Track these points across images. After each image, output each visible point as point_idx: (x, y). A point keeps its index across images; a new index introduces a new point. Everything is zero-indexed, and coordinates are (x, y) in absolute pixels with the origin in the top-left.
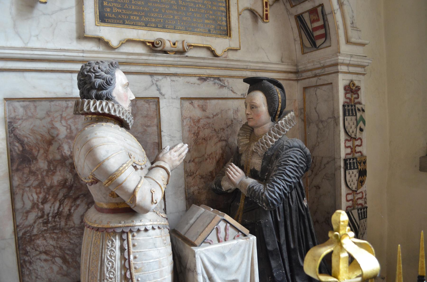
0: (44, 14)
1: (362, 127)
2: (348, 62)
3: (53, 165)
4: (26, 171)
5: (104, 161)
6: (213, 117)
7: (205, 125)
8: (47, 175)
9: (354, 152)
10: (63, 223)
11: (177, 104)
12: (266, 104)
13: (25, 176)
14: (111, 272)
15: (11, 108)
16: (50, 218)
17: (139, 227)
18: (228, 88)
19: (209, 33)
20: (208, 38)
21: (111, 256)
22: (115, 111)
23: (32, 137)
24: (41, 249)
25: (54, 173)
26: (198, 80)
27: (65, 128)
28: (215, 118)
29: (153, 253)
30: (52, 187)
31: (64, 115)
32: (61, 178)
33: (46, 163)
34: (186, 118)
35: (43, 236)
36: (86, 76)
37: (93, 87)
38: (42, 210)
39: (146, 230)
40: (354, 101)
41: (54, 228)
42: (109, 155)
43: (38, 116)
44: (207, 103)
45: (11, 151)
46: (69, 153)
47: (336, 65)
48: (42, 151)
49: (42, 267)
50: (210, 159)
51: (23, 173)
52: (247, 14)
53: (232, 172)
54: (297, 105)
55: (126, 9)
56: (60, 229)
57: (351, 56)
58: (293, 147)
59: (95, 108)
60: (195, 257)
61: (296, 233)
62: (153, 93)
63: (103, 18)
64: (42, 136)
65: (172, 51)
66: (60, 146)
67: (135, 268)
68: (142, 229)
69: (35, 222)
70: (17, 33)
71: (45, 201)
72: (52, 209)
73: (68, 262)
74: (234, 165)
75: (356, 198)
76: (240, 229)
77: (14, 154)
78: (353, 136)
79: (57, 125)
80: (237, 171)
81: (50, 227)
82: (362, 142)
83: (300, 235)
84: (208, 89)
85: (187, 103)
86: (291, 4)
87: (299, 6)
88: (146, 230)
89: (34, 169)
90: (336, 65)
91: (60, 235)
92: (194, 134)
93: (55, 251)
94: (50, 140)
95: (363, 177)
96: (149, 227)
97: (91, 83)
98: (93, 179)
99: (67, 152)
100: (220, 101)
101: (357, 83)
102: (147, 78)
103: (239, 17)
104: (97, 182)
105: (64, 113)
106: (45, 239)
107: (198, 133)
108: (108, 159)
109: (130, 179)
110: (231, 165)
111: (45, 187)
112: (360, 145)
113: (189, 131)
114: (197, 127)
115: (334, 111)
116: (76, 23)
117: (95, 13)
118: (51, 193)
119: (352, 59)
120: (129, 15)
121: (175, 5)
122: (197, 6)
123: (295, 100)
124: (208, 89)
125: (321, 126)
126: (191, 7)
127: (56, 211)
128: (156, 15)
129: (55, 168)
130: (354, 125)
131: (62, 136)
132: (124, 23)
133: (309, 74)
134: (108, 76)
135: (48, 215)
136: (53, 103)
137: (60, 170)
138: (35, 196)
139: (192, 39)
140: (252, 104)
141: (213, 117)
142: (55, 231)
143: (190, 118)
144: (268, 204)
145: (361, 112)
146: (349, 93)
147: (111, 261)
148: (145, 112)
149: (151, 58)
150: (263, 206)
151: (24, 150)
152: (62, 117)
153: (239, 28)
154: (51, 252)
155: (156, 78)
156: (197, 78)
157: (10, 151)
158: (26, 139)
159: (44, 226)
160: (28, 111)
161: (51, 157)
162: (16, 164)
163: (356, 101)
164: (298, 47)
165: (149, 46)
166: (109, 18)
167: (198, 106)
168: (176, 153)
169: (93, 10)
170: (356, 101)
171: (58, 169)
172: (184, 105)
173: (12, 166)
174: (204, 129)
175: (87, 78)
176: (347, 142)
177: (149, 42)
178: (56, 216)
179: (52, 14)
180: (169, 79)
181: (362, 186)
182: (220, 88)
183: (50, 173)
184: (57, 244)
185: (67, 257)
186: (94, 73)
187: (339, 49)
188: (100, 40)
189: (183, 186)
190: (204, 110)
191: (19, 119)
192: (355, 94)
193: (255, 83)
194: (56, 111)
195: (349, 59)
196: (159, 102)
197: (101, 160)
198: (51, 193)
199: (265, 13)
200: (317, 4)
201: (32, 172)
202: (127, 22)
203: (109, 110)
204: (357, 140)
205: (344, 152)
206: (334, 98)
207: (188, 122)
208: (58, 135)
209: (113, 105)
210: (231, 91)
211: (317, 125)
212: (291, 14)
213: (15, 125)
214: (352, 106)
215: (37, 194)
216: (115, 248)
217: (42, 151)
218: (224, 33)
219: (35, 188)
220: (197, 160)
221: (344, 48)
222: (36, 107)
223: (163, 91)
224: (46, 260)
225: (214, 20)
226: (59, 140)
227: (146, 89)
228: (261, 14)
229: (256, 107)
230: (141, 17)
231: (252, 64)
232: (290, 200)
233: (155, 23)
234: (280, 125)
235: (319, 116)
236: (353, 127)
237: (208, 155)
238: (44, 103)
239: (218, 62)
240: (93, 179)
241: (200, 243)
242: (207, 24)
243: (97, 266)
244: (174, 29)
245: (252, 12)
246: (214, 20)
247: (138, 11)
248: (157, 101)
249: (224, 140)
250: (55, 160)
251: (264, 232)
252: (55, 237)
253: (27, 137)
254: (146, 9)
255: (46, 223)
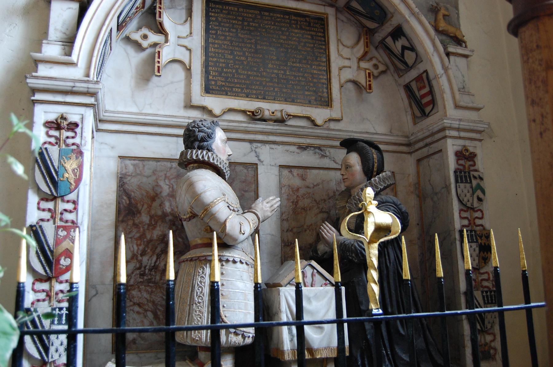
0: (157, 86)
1: (481, 196)
2: (457, 126)
3: (154, 220)
4: (131, 223)
5: (201, 194)
6: (314, 187)
7: (304, 194)
8: (148, 229)
9: (472, 224)
10: (158, 278)
11: (276, 170)
12: (360, 164)
13: (129, 227)
14: (200, 296)
15: (123, 165)
16: (147, 271)
17: (228, 258)
18: (330, 158)
19: (309, 103)
20: (307, 108)
21: (201, 282)
22: (213, 159)
23: (138, 193)
24: (136, 300)
25: (154, 228)
26: (298, 148)
27: (168, 186)
28: (315, 188)
29: (240, 284)
30: (151, 240)
31: (168, 175)
32: (160, 233)
33: (149, 217)
34: (285, 185)
35: (139, 287)
36: (191, 130)
37: (196, 139)
38: (140, 262)
39: (234, 262)
40: (469, 168)
41: (149, 281)
42: (206, 189)
43: (146, 174)
44: (307, 172)
45: (119, 203)
46: (170, 210)
47: (443, 129)
48: (145, 206)
49: (134, 319)
50: (310, 231)
51: (127, 225)
52: (350, 86)
53: (325, 231)
54: (411, 180)
55: (229, 82)
56: (154, 283)
57: (460, 120)
58: (386, 203)
59: (197, 156)
60: (279, 294)
61: (394, 298)
62: (251, 159)
63: (208, 90)
64: (147, 192)
65: (270, 120)
66: (162, 203)
67: (222, 295)
68: (231, 259)
69: (133, 273)
70: (135, 102)
71: (143, 254)
72: (150, 262)
73: (159, 318)
74: (328, 224)
75: (480, 279)
76: (328, 278)
77: (121, 206)
78: (469, 205)
79: (161, 183)
80: (330, 229)
81: (146, 280)
82: (483, 214)
83: (400, 300)
84: (307, 158)
85: (286, 172)
86: (398, 75)
87: (406, 76)
88: (234, 262)
89: (137, 222)
90: (443, 129)
91: (154, 290)
92: (293, 202)
93: (148, 304)
94: (154, 196)
95: (485, 253)
96: (237, 260)
97: (194, 136)
98: (191, 212)
99: (168, 209)
100: (321, 172)
101: (471, 150)
102: (247, 145)
103: (340, 89)
104: (194, 217)
105: (168, 173)
106: (140, 291)
107: (297, 202)
108: (205, 192)
109: (222, 211)
110: (325, 224)
111: (145, 240)
112: (482, 218)
113: (288, 199)
114: (295, 196)
115: (446, 178)
116: (184, 94)
117: (201, 85)
118: (150, 246)
119: (462, 123)
120: (232, 87)
121: (275, 78)
122: (298, 79)
123: (409, 175)
124: (307, 158)
125: (435, 199)
126: (291, 80)
127: (153, 265)
128: (257, 87)
129: (156, 223)
130: (470, 194)
131: (165, 194)
132: (227, 94)
133: (421, 144)
134: (209, 131)
135: (145, 267)
136: (159, 163)
137: (160, 225)
138: (136, 248)
139: (292, 109)
140: (347, 164)
141: (314, 187)
142: (150, 284)
143: (289, 186)
144: (357, 255)
145: (478, 181)
146: (462, 160)
147: (200, 287)
148: (243, 178)
149: (250, 125)
150: (353, 257)
151: (130, 203)
152: (166, 177)
153: (341, 99)
154: (144, 305)
155: (255, 145)
156: (297, 146)
157: (118, 203)
158: (133, 194)
159: (140, 278)
160: (137, 169)
161: (153, 212)
162: (123, 215)
163: (472, 168)
164: (410, 118)
165: (249, 115)
166: (213, 90)
167: (298, 174)
168: (268, 204)
169: (199, 83)
170: (472, 168)
171: (158, 224)
172: (283, 173)
173: (118, 217)
174: (304, 198)
175: (191, 133)
176: (462, 212)
177: (249, 112)
178: (152, 269)
179: (164, 86)
180: (268, 146)
181: (485, 263)
182: (320, 158)
183: (151, 228)
184: (151, 297)
185: (159, 313)
186: (198, 128)
187: (445, 113)
188: (203, 109)
189: (280, 256)
190: (304, 180)
191: (129, 176)
192: (469, 161)
193: (350, 144)
194: (162, 171)
195: (458, 123)
196: (257, 168)
197: (199, 193)
198: (150, 246)
199: (368, 83)
200: (422, 71)
201: (135, 225)
202: (229, 94)
203: (209, 158)
204: (477, 211)
205: (459, 223)
206: (444, 165)
207: (287, 191)
208: (161, 192)
209: (212, 155)
210: (333, 162)
211: (432, 199)
212: (400, 85)
213: (125, 181)
214: (465, 173)
215: (137, 245)
216: (205, 275)
217: (145, 206)
218: (325, 104)
219: (137, 239)
220: (295, 230)
221: (451, 112)
222: (144, 166)
223: (262, 158)
224: (138, 313)
225: (315, 91)
226: (162, 197)
227: (245, 155)
228: (364, 84)
229: (350, 167)
230: (242, 89)
231: (355, 135)
232: (388, 261)
233: (255, 94)
234: (373, 182)
235: (433, 188)
236: (468, 195)
237: (307, 226)
238: (151, 163)
239: (319, 131)
240: (191, 212)
241: (286, 283)
242: (307, 95)
243: (188, 292)
244: (274, 100)
245: (355, 83)
246: (315, 91)
247: (240, 84)
248: (254, 167)
249: (325, 212)
250: (156, 216)
251: (357, 291)
252: (150, 290)
253: (134, 192)
254: (248, 82)
255: (142, 275)
